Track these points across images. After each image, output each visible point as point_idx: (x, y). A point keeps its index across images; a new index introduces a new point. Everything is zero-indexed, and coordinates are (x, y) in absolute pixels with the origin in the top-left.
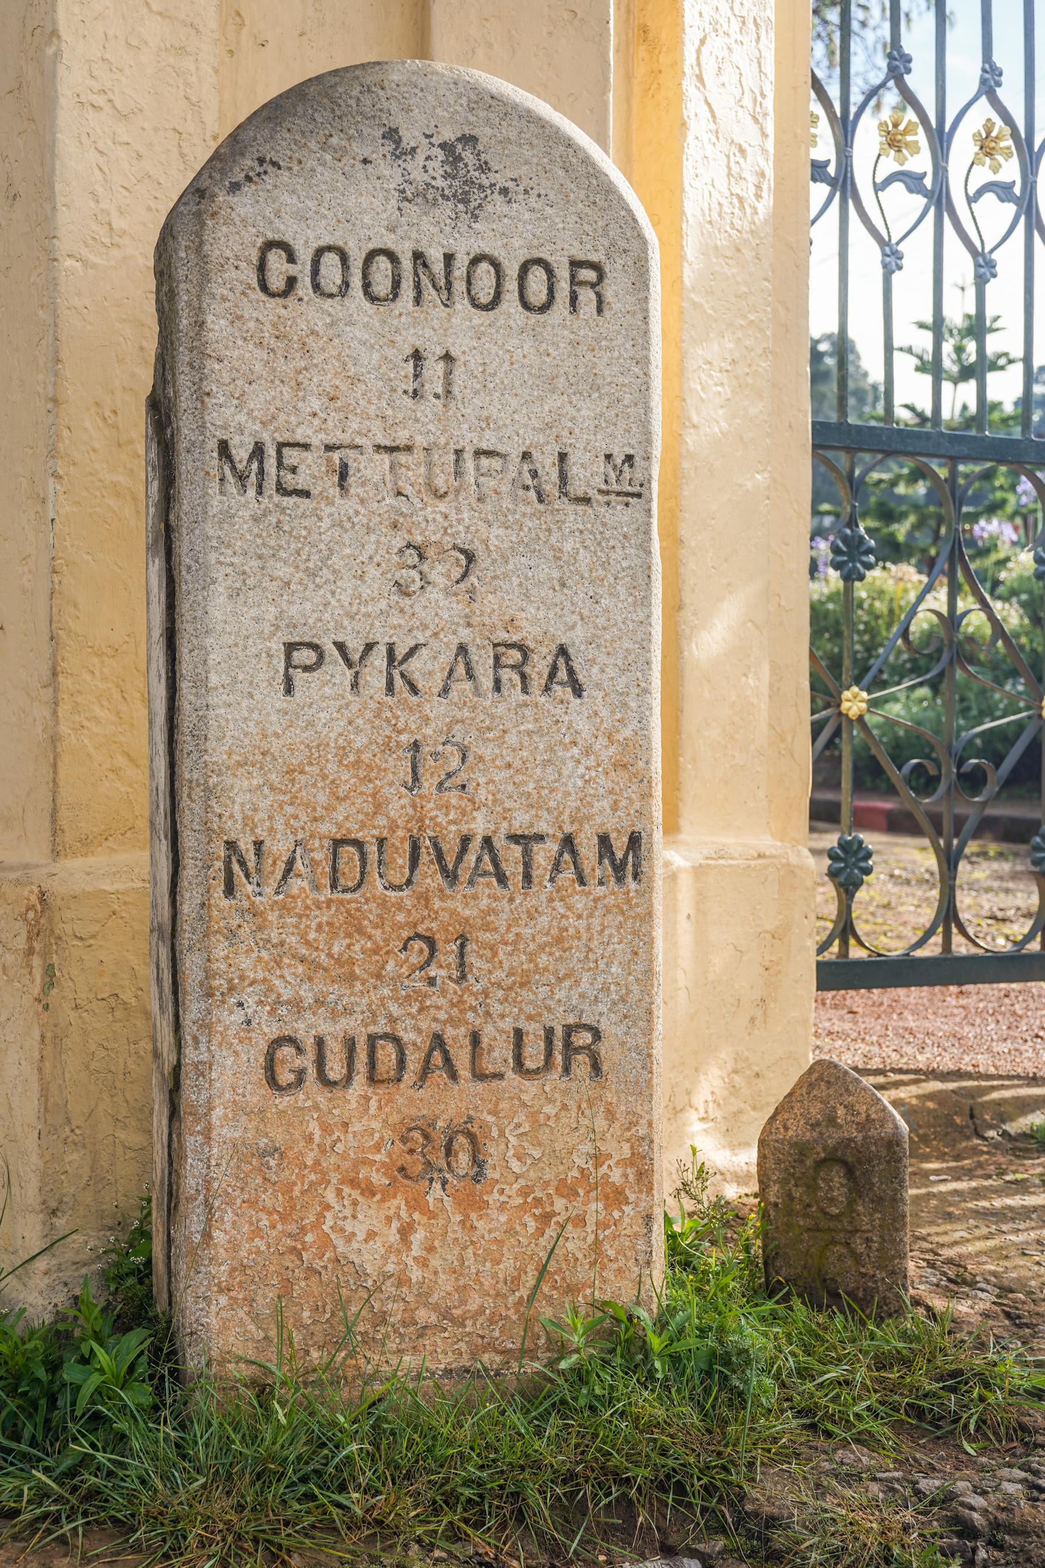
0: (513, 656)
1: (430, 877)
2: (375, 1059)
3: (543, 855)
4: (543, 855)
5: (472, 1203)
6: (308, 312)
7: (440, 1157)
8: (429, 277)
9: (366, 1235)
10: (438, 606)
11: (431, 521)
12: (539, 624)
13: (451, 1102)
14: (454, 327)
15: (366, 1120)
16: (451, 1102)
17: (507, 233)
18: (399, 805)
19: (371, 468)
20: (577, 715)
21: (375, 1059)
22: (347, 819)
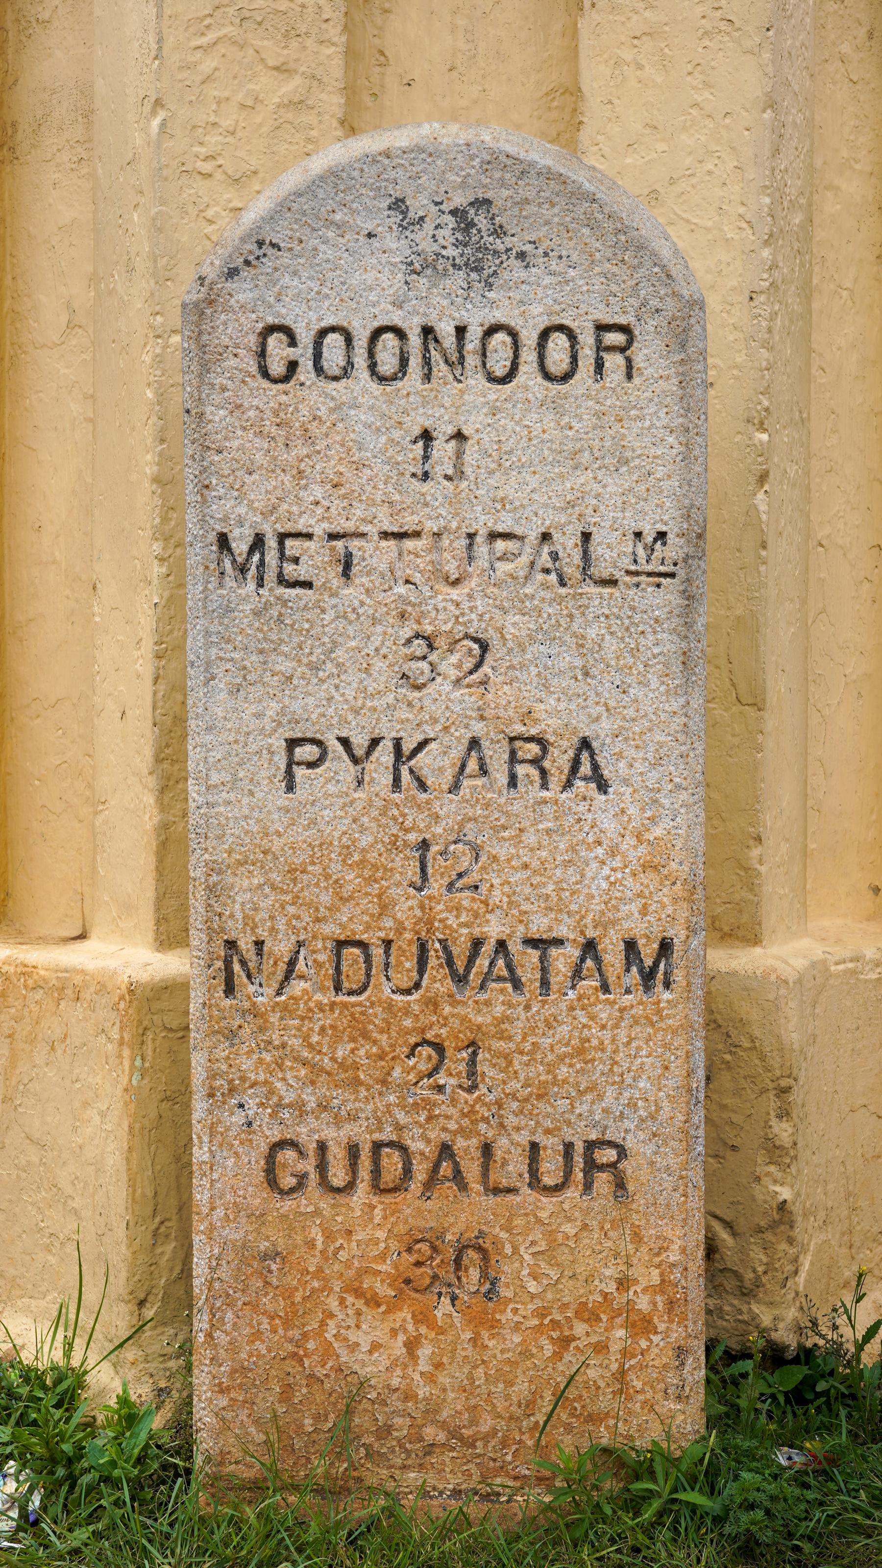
0: (529, 751)
1: (438, 981)
2: (379, 1165)
3: (562, 960)
4: (562, 960)
5: (483, 1321)
6: (311, 395)
7: (449, 1270)
8: (436, 350)
9: (370, 1345)
10: (447, 700)
11: (443, 609)
12: (558, 716)
13: (465, 1214)
14: (466, 401)
15: (370, 1228)
16: (465, 1214)
17: (526, 301)
18: (406, 908)
19: (376, 555)
20: (603, 813)
21: (379, 1165)
22: (351, 920)
